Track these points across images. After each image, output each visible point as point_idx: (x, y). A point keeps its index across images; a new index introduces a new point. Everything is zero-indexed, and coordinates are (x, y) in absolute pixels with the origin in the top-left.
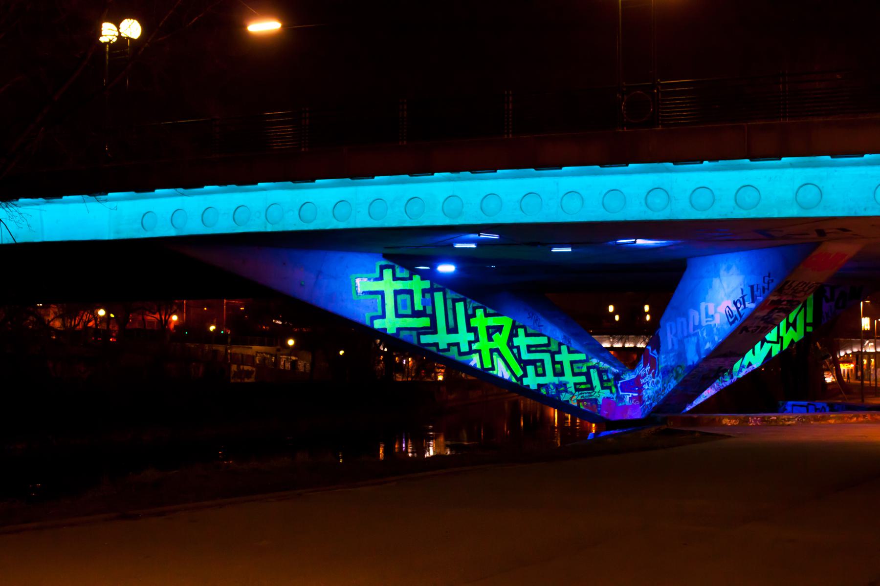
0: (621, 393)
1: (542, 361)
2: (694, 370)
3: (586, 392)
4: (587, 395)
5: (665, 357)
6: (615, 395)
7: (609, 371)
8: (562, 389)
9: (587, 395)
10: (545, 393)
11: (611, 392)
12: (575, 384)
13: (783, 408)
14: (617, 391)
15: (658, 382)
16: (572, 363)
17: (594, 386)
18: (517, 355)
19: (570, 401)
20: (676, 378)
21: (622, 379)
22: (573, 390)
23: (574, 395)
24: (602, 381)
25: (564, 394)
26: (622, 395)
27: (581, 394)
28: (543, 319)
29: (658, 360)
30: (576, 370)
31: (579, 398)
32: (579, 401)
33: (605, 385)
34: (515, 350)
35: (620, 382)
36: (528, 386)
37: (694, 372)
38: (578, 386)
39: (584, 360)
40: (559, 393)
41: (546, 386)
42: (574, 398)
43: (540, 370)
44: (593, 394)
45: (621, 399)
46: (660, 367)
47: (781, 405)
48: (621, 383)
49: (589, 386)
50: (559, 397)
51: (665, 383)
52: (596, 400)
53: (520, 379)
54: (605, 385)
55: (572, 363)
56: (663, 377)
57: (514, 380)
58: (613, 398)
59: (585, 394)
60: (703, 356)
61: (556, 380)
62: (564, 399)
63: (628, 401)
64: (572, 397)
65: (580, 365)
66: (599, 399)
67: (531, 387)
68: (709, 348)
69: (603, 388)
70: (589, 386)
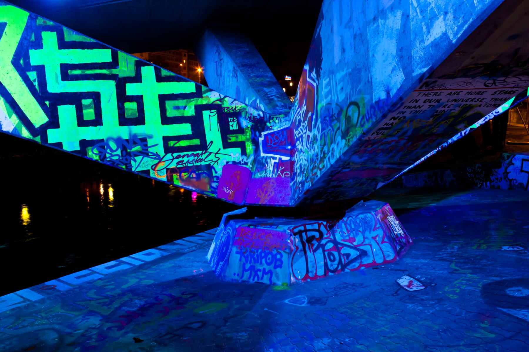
0: (262, 154)
1: (96, 97)
2: (390, 116)
3: (190, 153)
4: (191, 158)
5: (328, 84)
6: (252, 158)
7: (243, 114)
8: (137, 148)
9: (191, 158)
10: (96, 158)
11: (244, 153)
12: (166, 139)
13: (507, 162)
14: (256, 151)
15: (315, 138)
16: (163, 99)
17: (208, 142)
18: (36, 84)
19: (151, 171)
20: (345, 135)
21: (268, 129)
22: (160, 150)
23: (160, 160)
24: (225, 131)
25: (138, 159)
26: (263, 157)
27: (177, 157)
28: (225, 55)
29: (317, 90)
30: (171, 113)
31: (173, 165)
32: (171, 172)
33: (233, 139)
34: (33, 75)
35: (263, 134)
36: (60, 144)
37: (387, 120)
38: (171, 143)
39: (192, 93)
40: (127, 156)
41: (101, 144)
42: (161, 166)
43: (89, 114)
44: (204, 156)
45: (261, 164)
46: (319, 106)
47: (506, 158)
48: (266, 136)
49: (196, 142)
50: (129, 165)
51: (325, 145)
52: (210, 168)
53: (43, 131)
54: (233, 139)
55: (163, 99)
56: (323, 129)
57: (25, 134)
58: (246, 164)
59: (188, 159)
60: (420, 70)
61: (125, 132)
62: (139, 169)
63: (272, 169)
64: (156, 165)
65: (181, 103)
66: (215, 166)
67: (66, 148)
68: (445, 34)
69: (227, 144)
70: (196, 142)
